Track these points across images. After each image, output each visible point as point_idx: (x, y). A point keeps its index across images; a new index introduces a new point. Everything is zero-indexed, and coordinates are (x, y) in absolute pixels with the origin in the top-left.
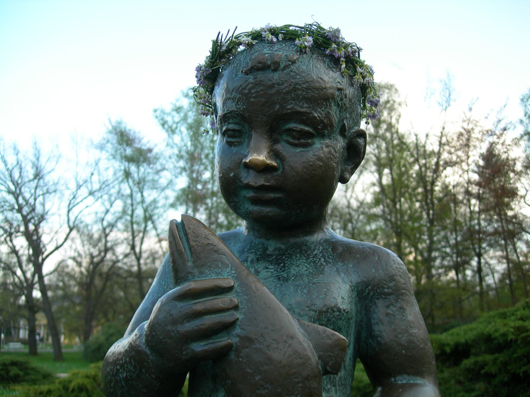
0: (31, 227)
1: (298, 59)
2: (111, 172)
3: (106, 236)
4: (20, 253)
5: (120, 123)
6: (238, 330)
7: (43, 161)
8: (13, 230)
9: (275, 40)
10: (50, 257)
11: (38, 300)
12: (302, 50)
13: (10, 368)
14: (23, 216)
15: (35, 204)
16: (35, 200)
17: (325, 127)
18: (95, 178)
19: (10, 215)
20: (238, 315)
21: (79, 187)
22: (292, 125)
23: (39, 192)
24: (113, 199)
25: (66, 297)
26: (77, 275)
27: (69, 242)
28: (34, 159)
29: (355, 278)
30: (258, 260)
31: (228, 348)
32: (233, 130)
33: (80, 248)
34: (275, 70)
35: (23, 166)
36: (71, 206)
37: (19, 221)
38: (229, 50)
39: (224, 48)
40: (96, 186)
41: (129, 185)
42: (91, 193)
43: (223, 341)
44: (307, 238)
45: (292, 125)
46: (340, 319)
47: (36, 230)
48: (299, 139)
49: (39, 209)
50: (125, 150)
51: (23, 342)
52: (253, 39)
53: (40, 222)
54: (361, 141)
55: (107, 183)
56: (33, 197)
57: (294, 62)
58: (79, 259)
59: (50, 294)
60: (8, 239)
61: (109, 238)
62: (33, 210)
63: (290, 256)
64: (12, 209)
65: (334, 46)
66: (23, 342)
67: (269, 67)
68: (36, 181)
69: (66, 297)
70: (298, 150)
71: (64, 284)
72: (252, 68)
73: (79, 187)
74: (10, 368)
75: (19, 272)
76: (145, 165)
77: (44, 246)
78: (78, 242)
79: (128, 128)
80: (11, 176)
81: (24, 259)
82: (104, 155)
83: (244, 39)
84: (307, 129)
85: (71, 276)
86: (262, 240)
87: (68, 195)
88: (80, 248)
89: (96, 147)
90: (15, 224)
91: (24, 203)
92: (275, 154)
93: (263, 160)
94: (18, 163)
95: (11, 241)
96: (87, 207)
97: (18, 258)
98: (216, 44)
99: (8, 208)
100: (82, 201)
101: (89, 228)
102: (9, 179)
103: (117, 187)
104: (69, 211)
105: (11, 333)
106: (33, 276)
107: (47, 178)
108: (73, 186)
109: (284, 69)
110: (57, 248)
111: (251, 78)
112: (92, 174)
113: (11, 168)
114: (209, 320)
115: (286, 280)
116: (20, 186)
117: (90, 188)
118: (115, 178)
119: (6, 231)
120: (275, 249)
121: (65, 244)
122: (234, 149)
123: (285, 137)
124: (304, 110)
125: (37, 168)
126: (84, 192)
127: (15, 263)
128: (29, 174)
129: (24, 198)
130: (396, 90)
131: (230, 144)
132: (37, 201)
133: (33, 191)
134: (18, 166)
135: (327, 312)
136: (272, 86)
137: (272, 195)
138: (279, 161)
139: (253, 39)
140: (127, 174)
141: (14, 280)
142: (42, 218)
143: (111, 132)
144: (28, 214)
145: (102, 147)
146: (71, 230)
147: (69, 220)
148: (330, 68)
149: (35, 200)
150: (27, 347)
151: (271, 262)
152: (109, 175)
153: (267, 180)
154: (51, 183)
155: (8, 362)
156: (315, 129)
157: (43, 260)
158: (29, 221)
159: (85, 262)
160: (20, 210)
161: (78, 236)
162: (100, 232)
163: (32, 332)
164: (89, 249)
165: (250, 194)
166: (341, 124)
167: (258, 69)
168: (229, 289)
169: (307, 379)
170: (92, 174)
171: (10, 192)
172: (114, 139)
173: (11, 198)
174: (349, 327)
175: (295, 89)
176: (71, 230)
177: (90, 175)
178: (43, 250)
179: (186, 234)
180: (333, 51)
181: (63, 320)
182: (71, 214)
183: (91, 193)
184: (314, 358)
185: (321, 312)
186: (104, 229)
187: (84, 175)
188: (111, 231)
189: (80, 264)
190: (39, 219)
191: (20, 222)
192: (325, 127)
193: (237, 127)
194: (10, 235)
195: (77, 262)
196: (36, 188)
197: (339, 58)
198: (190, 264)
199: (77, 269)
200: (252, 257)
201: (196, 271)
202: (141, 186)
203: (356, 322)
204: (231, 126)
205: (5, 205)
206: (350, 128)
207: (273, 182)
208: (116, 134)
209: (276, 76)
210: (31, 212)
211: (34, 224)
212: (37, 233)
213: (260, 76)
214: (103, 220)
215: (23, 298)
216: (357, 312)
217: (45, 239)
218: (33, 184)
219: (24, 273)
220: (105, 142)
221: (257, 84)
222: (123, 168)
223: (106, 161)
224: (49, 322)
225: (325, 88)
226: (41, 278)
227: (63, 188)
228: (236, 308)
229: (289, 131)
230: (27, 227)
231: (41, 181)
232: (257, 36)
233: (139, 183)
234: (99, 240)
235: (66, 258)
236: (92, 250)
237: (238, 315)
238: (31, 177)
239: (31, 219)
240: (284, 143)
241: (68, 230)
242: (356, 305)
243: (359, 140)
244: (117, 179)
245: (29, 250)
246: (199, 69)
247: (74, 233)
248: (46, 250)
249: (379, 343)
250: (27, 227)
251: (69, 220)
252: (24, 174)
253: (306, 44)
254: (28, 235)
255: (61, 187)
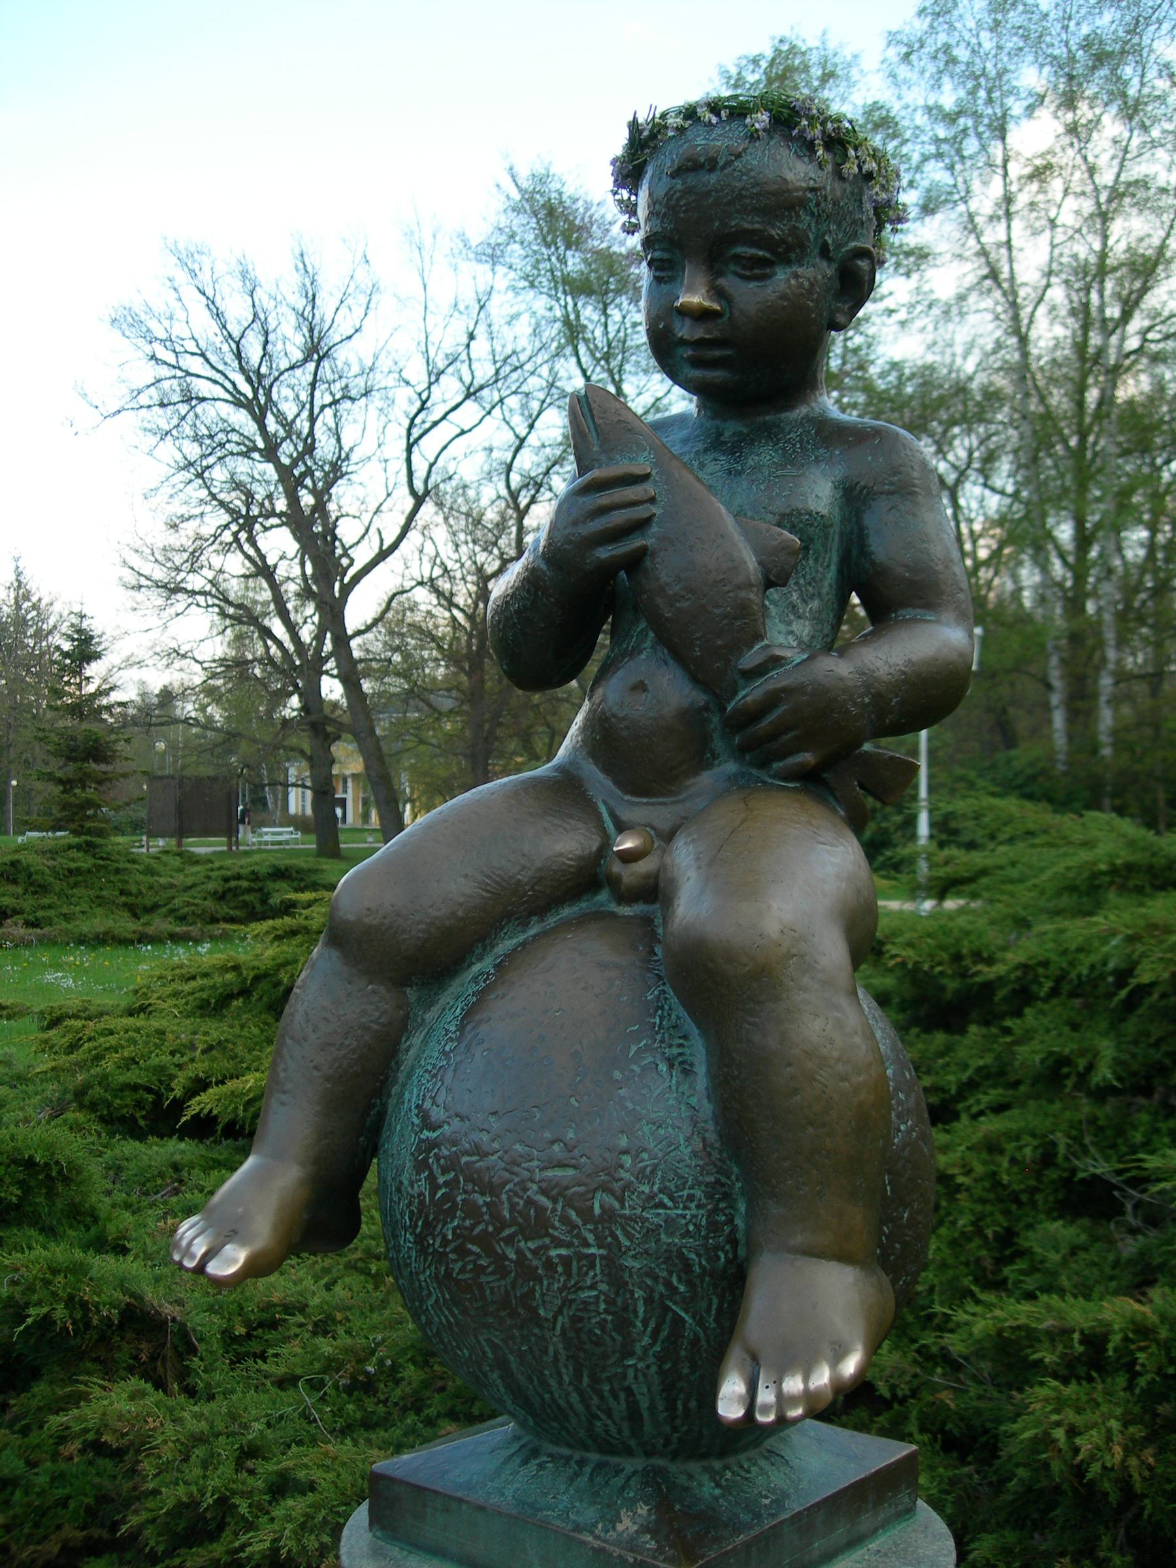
0: (307, 499)
1: (745, 150)
2: (524, 327)
3: (522, 514)
4: (281, 573)
5: (542, 179)
6: (654, 529)
7: (326, 306)
8: (255, 511)
9: (714, 120)
10: (365, 581)
11: (335, 705)
12: (753, 137)
13: (271, 885)
14: (279, 466)
15: (311, 433)
16: (312, 420)
17: (790, 248)
18: (480, 347)
19: (242, 467)
20: (656, 510)
21: (435, 376)
22: (740, 250)
23: (322, 397)
24: (535, 405)
25: (417, 694)
26: (443, 630)
27: (414, 536)
28: (300, 303)
29: (839, 472)
30: (706, 450)
31: (643, 552)
32: (661, 260)
33: (447, 552)
34: (712, 170)
35: (272, 324)
36: (416, 432)
37: (268, 482)
38: (653, 136)
39: (646, 133)
40: (484, 371)
41: (579, 362)
42: (471, 393)
43: (635, 543)
44: (783, 415)
45: (740, 250)
46: (811, 525)
47: (320, 507)
48: (751, 269)
49: (325, 448)
50: (563, 261)
51: (299, 823)
52: (686, 118)
53: (329, 485)
54: (863, 264)
55: (514, 361)
56: (305, 414)
57: (738, 156)
58: (444, 585)
59: (367, 686)
60: (243, 536)
61: (527, 522)
62: (310, 449)
63: (752, 441)
64: (248, 451)
65: (805, 122)
66: (299, 823)
67: (702, 166)
68: (311, 366)
69: (417, 694)
70: (752, 285)
71: (407, 656)
72: (679, 168)
73: (435, 376)
74: (271, 885)
75: (278, 628)
76: (624, 300)
77: (345, 554)
78: (441, 534)
79: (569, 191)
80: (239, 356)
81: (292, 588)
82: (503, 278)
83: (671, 121)
84: (761, 253)
85: (427, 636)
86: (718, 422)
87: (405, 401)
88: (447, 552)
89: (479, 257)
90: (260, 493)
91: (282, 433)
92: (718, 293)
93: (700, 304)
94: (255, 315)
95: (252, 540)
96: (463, 432)
97: (275, 587)
98: (634, 126)
99: (237, 449)
100: (444, 417)
101: (471, 493)
102: (236, 364)
103: (544, 371)
104: (409, 449)
105: (265, 804)
106: (319, 638)
107: (342, 354)
108: (418, 375)
109: (723, 168)
110: (383, 555)
111: (679, 184)
112: (472, 337)
113: (236, 334)
114: (618, 518)
115: (739, 473)
116: (267, 382)
117: (467, 379)
118: (538, 345)
119: (234, 513)
120: (734, 434)
121: (404, 544)
122: (665, 288)
123: (732, 267)
124: (757, 226)
125: (311, 330)
126: (449, 390)
127: (265, 604)
128: (289, 347)
129: (280, 417)
130: (781, 41)
131: (658, 280)
132: (318, 424)
133: (304, 396)
134: (257, 326)
135: (790, 514)
136: (708, 194)
137: (717, 353)
138: (724, 303)
139: (686, 118)
140: (573, 331)
141: (267, 648)
142: (335, 472)
143: (517, 210)
144: (295, 463)
145: (493, 255)
146: (419, 501)
147: (410, 474)
148: (799, 157)
149: (312, 420)
150: (313, 837)
151: (724, 452)
152: (519, 336)
153: (708, 331)
154: (355, 370)
155: (263, 870)
156: (773, 252)
157: (347, 590)
158: (299, 482)
159: (463, 595)
160: (270, 453)
161: (440, 519)
162: (502, 504)
163: (325, 795)
164: (472, 557)
165: (688, 352)
166: (820, 241)
167: (688, 170)
168: (645, 477)
169: (739, 588)
170: (472, 337)
171: (239, 402)
172: (527, 227)
173: (242, 420)
174: (826, 538)
175: (740, 197)
176: (419, 501)
177: (464, 339)
178: (345, 562)
179: (591, 410)
180: (803, 131)
181: (408, 761)
182: (415, 457)
183: (471, 393)
184: (751, 562)
185: (783, 515)
186: (514, 495)
187: (450, 338)
188: (533, 500)
189: (448, 600)
190: (326, 474)
191: (272, 488)
192: (790, 248)
193: (666, 256)
194: (248, 523)
195: (439, 593)
196: (313, 385)
197: (812, 141)
198: (596, 448)
199: (442, 614)
200: (700, 446)
201: (603, 457)
202: (614, 364)
203: (841, 534)
204: (657, 254)
205: (228, 441)
206: (839, 246)
207: (716, 334)
208: (535, 214)
209: (713, 178)
210: (301, 456)
211: (313, 491)
212: (325, 515)
213: (691, 179)
214: (509, 468)
215: (295, 701)
216: (843, 520)
217: (347, 531)
218: (305, 375)
219: (292, 628)
220: (502, 239)
221: (688, 191)
222: (558, 313)
223: (511, 294)
224: (367, 767)
225: (789, 191)
226: (342, 640)
227: (390, 381)
228: (652, 500)
229: (737, 258)
230: (294, 500)
231: (326, 364)
232: (690, 113)
233: (607, 357)
234: (501, 526)
235: (408, 584)
236: (481, 557)
237: (656, 510)
238: (298, 355)
239: (303, 475)
240: (731, 277)
241: (410, 503)
242: (841, 509)
243: (860, 263)
244: (543, 347)
245: (302, 564)
246: (614, 162)
247: (428, 508)
248: (351, 564)
249: (873, 563)
250: (294, 500)
251: (410, 474)
252: (275, 349)
253: (757, 126)
254: (297, 521)
255: (380, 379)
